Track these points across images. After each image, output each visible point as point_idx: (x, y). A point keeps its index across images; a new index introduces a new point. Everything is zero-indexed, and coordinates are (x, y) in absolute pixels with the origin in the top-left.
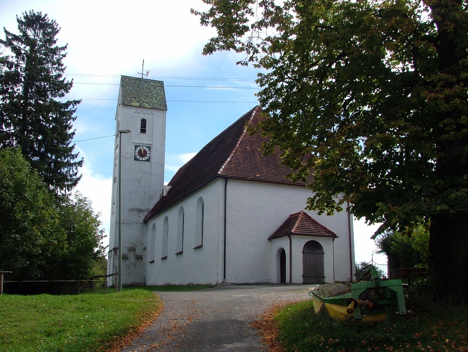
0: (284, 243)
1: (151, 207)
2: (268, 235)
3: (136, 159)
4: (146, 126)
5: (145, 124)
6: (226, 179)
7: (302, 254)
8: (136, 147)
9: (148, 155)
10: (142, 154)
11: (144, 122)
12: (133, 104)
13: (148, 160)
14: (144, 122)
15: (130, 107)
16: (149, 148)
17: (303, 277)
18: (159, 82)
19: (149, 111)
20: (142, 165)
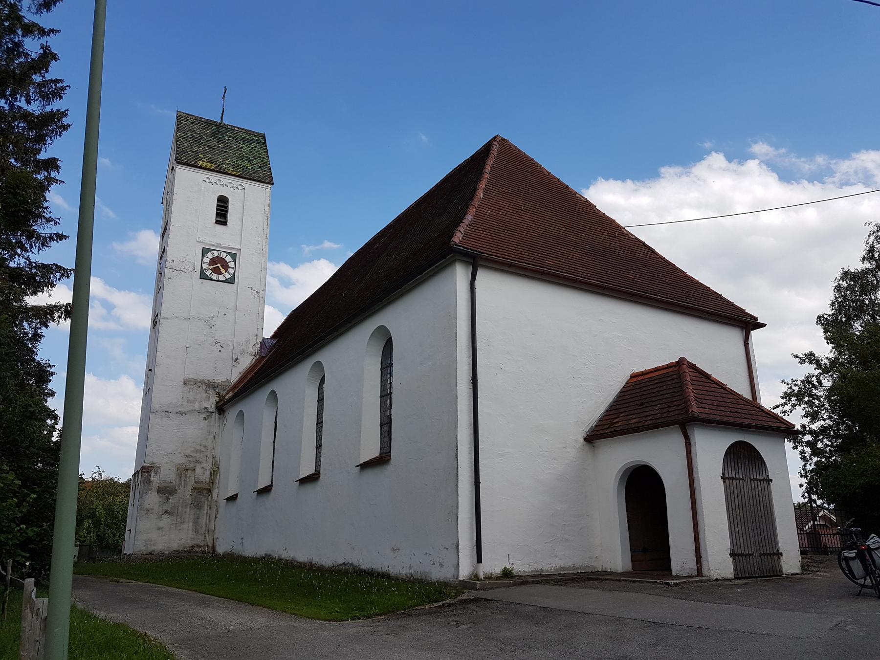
0: (660, 452)
1: (235, 378)
2: (190, 376)
3: (203, 276)
4: (227, 211)
5: (227, 207)
6: (476, 261)
7: (721, 482)
8: (205, 251)
9: (229, 270)
10: (219, 264)
11: (223, 205)
12: (200, 163)
13: (231, 281)
14: (223, 205)
15: (359, 609)
16: (234, 256)
17: (733, 555)
18: (259, 135)
19: (237, 182)
20: (214, 290)
